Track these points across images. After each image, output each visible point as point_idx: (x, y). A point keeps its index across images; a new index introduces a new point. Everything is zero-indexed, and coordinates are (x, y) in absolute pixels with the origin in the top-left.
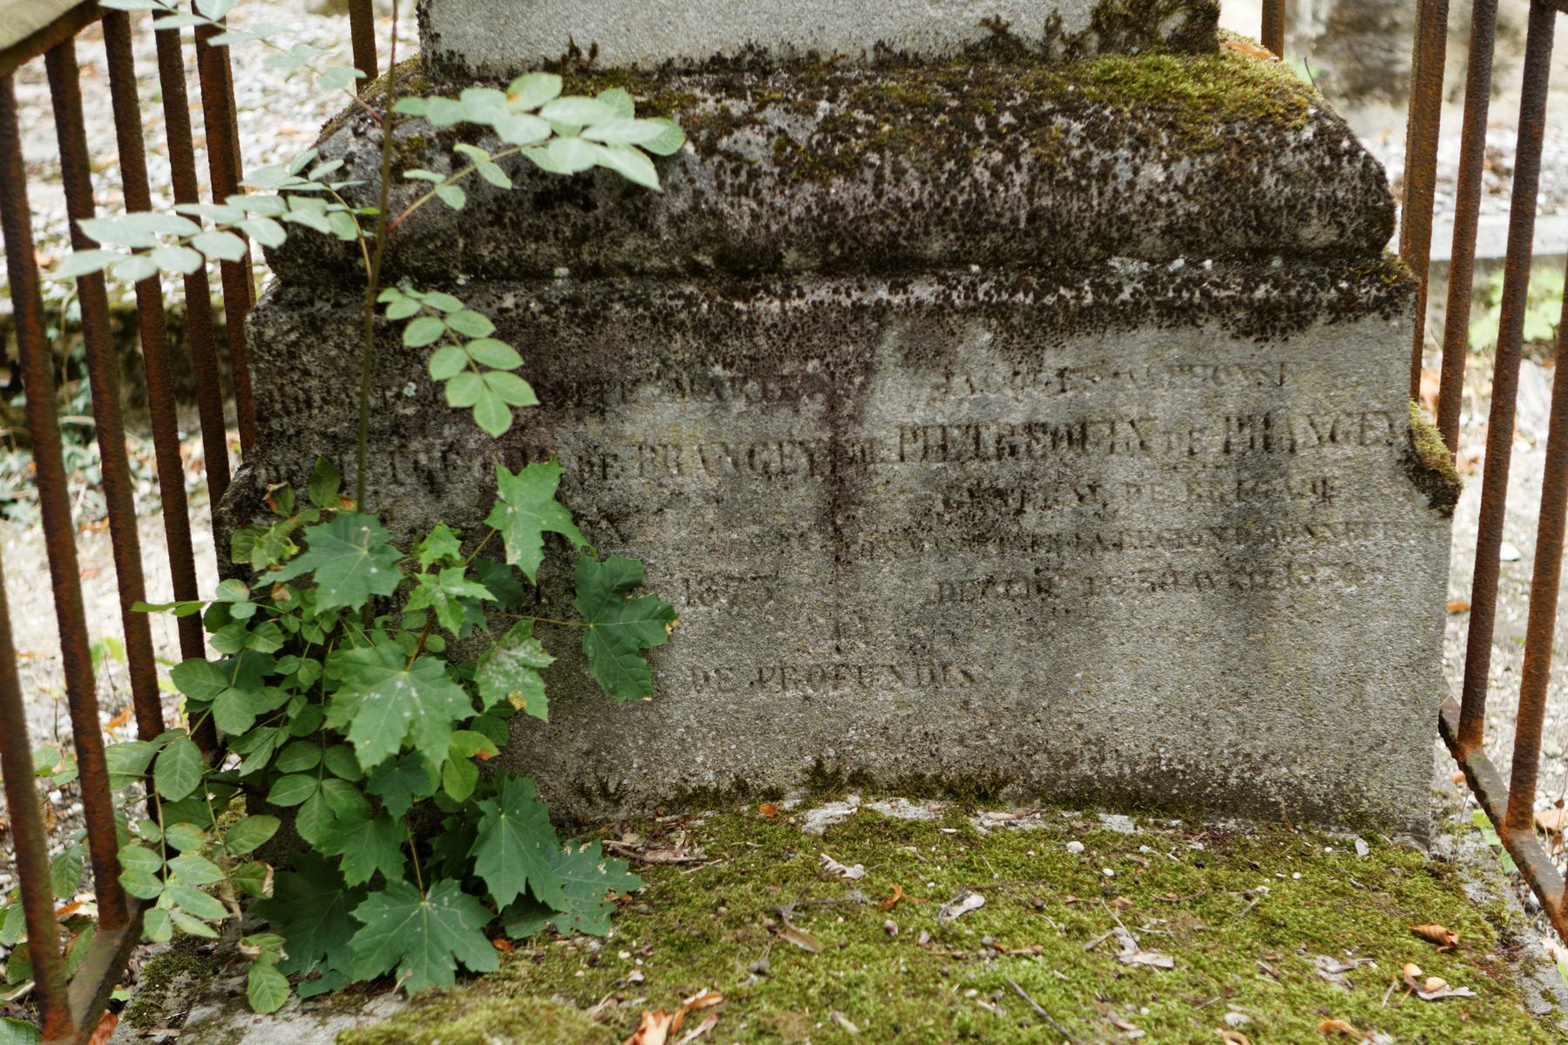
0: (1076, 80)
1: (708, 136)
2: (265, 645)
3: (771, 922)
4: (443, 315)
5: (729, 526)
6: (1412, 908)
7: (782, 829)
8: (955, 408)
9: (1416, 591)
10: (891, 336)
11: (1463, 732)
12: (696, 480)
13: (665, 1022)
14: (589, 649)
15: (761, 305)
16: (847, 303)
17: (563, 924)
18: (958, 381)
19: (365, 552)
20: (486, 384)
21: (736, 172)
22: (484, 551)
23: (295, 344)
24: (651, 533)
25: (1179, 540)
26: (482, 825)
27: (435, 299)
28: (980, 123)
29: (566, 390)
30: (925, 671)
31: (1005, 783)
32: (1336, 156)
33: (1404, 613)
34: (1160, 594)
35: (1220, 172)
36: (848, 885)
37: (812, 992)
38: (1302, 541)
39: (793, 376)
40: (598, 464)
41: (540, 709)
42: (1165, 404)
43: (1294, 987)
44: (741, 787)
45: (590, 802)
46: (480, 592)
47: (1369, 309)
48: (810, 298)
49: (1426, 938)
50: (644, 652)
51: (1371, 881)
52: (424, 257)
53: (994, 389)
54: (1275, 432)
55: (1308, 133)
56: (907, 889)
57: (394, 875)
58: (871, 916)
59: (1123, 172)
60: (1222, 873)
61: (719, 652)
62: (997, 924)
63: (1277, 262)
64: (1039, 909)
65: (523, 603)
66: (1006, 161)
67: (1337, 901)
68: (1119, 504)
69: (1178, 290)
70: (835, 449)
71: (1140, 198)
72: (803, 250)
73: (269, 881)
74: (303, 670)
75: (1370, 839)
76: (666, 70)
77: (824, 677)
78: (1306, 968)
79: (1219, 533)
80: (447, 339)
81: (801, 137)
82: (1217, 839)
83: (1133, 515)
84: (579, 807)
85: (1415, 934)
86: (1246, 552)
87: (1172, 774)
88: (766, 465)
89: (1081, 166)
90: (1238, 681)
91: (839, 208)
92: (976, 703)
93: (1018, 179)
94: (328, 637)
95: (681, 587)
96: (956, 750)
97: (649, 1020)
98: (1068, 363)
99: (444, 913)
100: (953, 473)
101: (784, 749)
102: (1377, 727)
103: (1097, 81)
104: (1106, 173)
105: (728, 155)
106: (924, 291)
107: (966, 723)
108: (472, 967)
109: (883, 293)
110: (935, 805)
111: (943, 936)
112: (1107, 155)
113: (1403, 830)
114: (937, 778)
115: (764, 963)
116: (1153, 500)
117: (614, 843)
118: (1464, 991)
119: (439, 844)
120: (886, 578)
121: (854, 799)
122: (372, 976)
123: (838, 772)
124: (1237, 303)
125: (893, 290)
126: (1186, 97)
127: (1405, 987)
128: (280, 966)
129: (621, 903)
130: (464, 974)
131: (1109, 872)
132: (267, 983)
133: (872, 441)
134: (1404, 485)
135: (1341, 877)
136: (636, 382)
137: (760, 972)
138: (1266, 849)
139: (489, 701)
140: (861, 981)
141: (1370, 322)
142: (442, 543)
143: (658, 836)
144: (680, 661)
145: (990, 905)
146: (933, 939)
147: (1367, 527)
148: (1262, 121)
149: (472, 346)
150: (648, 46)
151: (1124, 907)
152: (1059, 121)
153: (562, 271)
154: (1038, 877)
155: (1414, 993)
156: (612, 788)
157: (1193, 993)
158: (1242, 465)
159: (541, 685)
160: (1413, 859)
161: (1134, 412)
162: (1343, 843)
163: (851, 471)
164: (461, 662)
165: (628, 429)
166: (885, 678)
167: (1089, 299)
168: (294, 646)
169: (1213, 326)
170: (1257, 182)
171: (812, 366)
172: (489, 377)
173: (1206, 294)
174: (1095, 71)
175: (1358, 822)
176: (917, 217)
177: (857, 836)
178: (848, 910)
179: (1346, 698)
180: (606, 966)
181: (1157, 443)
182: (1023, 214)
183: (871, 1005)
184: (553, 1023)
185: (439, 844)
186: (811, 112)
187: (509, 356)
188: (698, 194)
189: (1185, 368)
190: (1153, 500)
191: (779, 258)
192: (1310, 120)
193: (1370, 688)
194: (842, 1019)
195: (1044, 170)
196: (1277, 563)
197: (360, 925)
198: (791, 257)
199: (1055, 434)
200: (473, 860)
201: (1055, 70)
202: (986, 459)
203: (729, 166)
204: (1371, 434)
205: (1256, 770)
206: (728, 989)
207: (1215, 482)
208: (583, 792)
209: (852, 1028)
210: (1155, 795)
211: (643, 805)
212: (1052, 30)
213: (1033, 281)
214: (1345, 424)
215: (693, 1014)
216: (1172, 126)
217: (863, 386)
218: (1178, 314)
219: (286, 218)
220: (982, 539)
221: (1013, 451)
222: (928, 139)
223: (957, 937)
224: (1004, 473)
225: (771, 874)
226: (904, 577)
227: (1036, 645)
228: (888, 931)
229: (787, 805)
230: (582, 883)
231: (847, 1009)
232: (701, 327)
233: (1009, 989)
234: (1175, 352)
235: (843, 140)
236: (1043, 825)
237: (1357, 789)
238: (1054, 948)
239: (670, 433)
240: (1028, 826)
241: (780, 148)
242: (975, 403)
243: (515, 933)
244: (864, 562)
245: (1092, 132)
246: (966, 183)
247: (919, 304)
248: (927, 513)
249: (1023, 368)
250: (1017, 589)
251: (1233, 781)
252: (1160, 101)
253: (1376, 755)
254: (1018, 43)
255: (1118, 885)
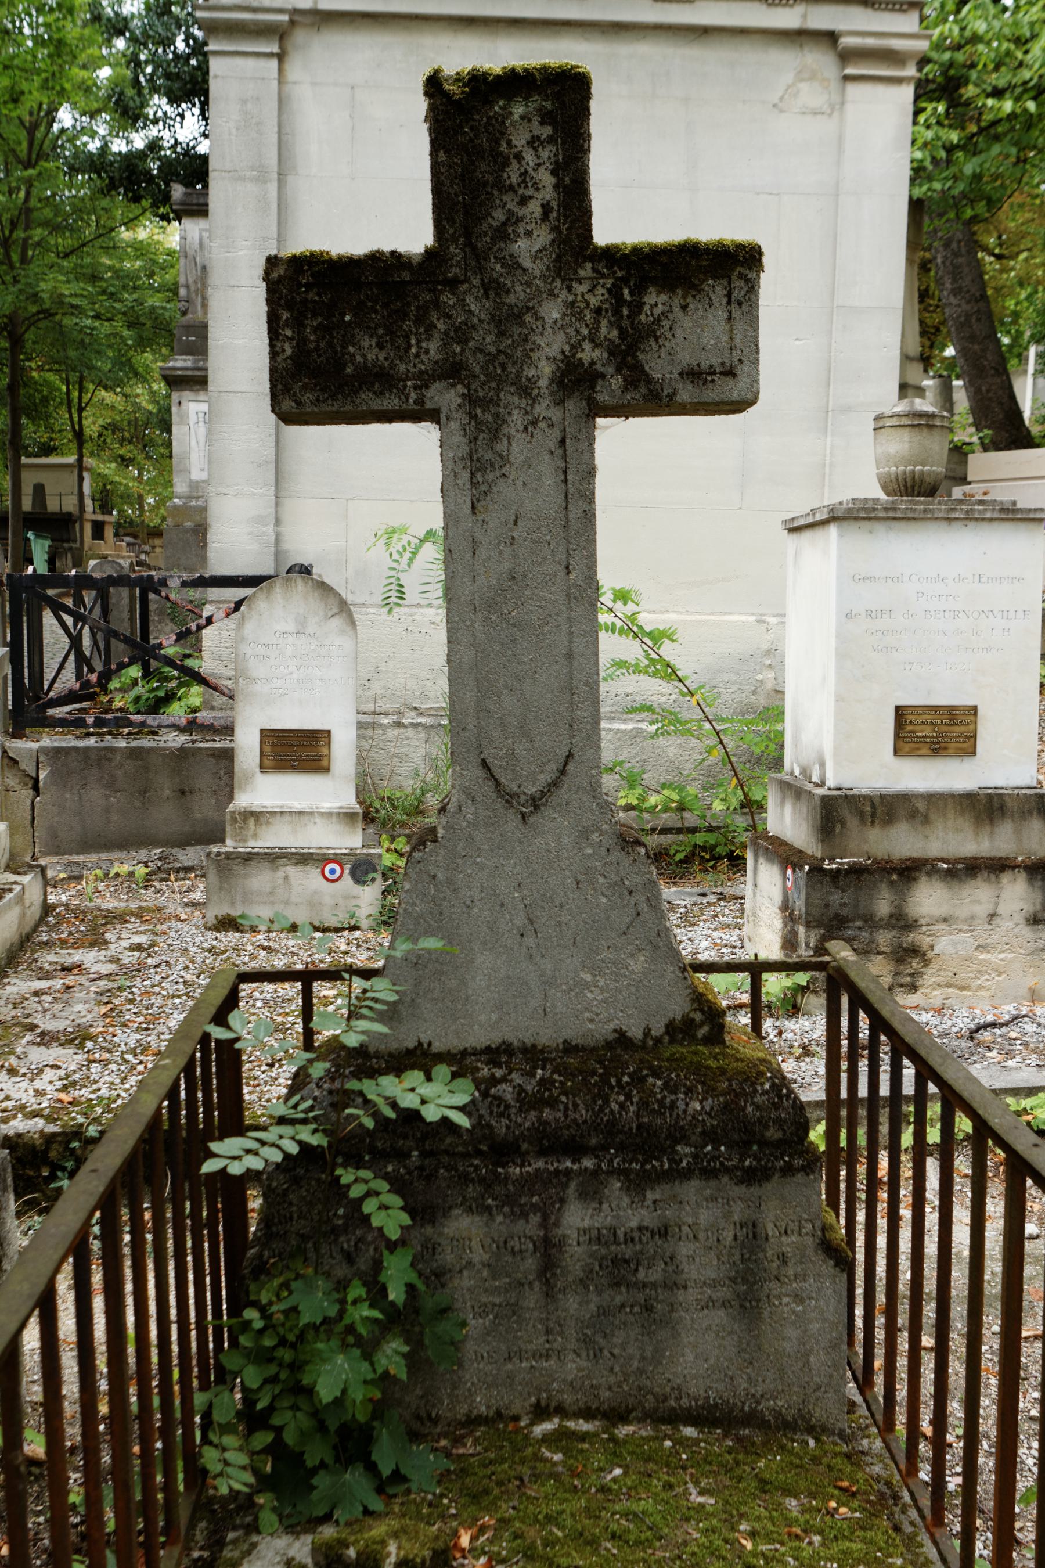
0: (658, 1059)
1: (485, 1087)
2: (268, 1342)
3: (518, 1483)
4: (366, 1182)
5: (494, 1278)
6: (835, 1474)
7: (520, 1437)
8: (604, 1219)
9: (831, 1308)
10: (573, 1185)
11: (865, 1383)
12: (478, 1255)
13: (469, 1533)
14: (427, 1342)
15: (511, 1170)
16: (552, 1169)
17: (414, 1487)
18: (605, 1206)
19: (320, 1294)
20: (389, 1216)
21: (499, 1106)
22: (377, 1293)
23: (287, 1189)
24: (456, 1282)
25: (714, 1284)
26: (375, 1433)
27: (364, 1174)
28: (613, 1081)
29: (423, 1212)
30: (591, 1352)
31: (632, 1411)
32: (780, 1096)
33: (825, 1320)
34: (706, 1311)
35: (726, 1105)
36: (555, 1464)
37: (540, 1517)
38: (774, 1284)
39: (525, 1204)
40: (430, 1248)
41: (403, 1376)
42: (705, 1216)
43: (774, 1513)
44: (499, 1414)
45: (422, 1423)
46: (376, 1314)
47: (799, 1170)
48: (534, 1166)
49: (841, 1489)
50: (452, 1343)
51: (816, 1460)
52: (351, 1147)
53: (625, 1211)
54: (758, 1230)
55: (767, 1086)
56: (584, 1466)
57: (329, 1460)
58: (567, 1479)
59: (681, 1105)
60: (741, 1457)
61: (489, 1344)
62: (629, 1483)
63: (755, 1148)
64: (650, 1476)
65: (397, 1319)
66: (626, 1100)
67: (798, 1470)
68: (685, 1266)
69: (709, 1162)
70: (546, 1240)
71: (689, 1118)
72: (530, 1143)
73: (269, 1465)
74: (286, 1355)
75: (817, 1440)
76: (464, 1053)
77: (541, 1356)
78: (780, 1504)
79: (733, 1280)
80: (369, 1194)
81: (529, 1088)
82: (739, 1440)
83: (691, 1272)
84: (416, 1426)
85: (836, 1487)
86: (747, 1289)
87: (716, 1405)
88: (513, 1248)
89: (661, 1102)
90: (747, 1356)
91: (547, 1123)
92: (617, 1369)
93: (632, 1109)
94: (297, 1337)
95: (470, 1309)
96: (607, 1394)
97: (462, 1531)
98: (658, 1197)
99: (355, 1478)
100: (603, 1252)
101: (521, 1394)
102: (817, 1379)
103: (668, 1060)
104: (673, 1105)
105: (495, 1097)
106: (588, 1163)
107: (612, 1379)
108: (371, 1508)
109: (568, 1164)
110: (597, 1423)
111: (603, 1489)
112: (673, 1097)
113: (833, 1434)
114: (598, 1409)
115: (516, 1503)
116: (700, 1265)
117: (436, 1445)
118: (857, 1515)
119: (353, 1444)
120: (571, 1303)
121: (556, 1420)
122: (321, 1514)
123: (548, 1406)
124: (736, 1168)
125: (573, 1162)
126: (708, 1068)
127: (828, 1513)
128: (274, 1509)
129: (442, 1475)
130: (367, 1512)
131: (684, 1456)
132: (268, 1518)
133: (564, 1236)
134: (821, 1256)
135: (801, 1459)
136: (450, 1208)
137: (514, 1508)
138: (764, 1444)
139: (380, 1371)
140: (563, 1511)
141: (800, 1177)
142: (357, 1290)
143: (458, 1441)
144: (470, 1348)
145: (626, 1473)
146: (597, 1491)
147: (804, 1277)
148: (745, 1080)
149: (381, 1197)
150: (456, 1042)
151: (692, 1474)
152: (651, 1080)
153: (415, 1153)
154: (648, 1459)
155: (833, 1516)
156: (433, 1415)
157: (724, 1516)
158: (743, 1246)
159: (403, 1362)
160: (838, 1449)
161: (690, 1221)
162: (803, 1441)
163: (554, 1251)
164: (368, 1350)
165: (446, 1230)
166: (571, 1356)
167: (667, 1166)
168: (282, 1342)
169: (725, 1179)
170: (744, 1109)
171: (535, 1199)
172: (390, 1211)
173: (722, 1163)
174: (667, 1055)
175: (811, 1430)
176: (584, 1127)
177: (559, 1439)
178: (557, 1477)
179: (800, 1364)
180: (437, 1507)
181: (701, 1236)
182: (634, 1126)
183: (569, 1522)
184: (417, 1532)
185: (353, 1444)
186: (534, 1075)
187: (397, 1201)
188: (481, 1117)
189: (713, 1199)
190: (700, 1265)
191: (519, 1147)
192: (768, 1079)
193: (812, 1359)
194: (555, 1530)
195: (644, 1104)
196: (762, 1295)
197: (315, 1488)
198: (525, 1146)
199: (652, 1232)
200: (370, 1453)
201: (648, 1054)
202: (619, 1244)
203: (496, 1103)
204: (804, 1231)
205: (758, 1403)
206: (499, 1516)
207: (730, 1255)
208: (418, 1418)
209: (560, 1534)
210: (707, 1416)
211: (449, 1425)
212: (647, 1033)
213: (640, 1157)
214: (791, 1226)
215: (482, 1529)
216: (703, 1083)
217: (559, 1209)
218: (709, 1174)
219: (297, 1137)
220: (618, 1284)
221: (632, 1240)
222: (589, 1090)
223: (610, 1490)
224: (628, 1251)
225: (517, 1459)
226: (580, 1304)
227: (646, 1338)
228: (576, 1487)
229: (522, 1424)
230: (424, 1464)
231: (557, 1525)
232: (482, 1180)
233: (635, 1515)
234: (708, 1191)
235: (549, 1090)
236: (652, 1433)
237: (809, 1412)
238: (657, 1494)
239: (466, 1231)
240: (644, 1433)
241: (519, 1094)
242: (613, 1217)
243: (391, 1491)
244: (561, 1296)
245: (666, 1086)
246: (607, 1111)
247: (586, 1169)
248: (591, 1271)
249: (636, 1200)
250: (636, 1309)
251: (747, 1408)
252: (697, 1069)
253: (818, 1394)
254: (630, 1039)
255: (689, 1464)
